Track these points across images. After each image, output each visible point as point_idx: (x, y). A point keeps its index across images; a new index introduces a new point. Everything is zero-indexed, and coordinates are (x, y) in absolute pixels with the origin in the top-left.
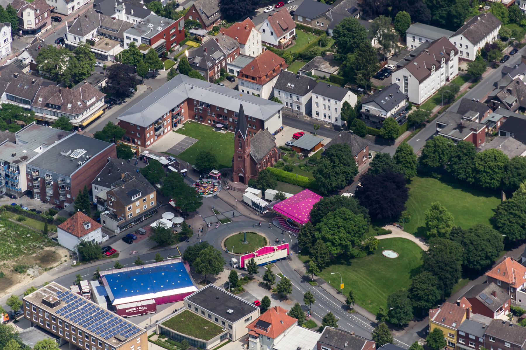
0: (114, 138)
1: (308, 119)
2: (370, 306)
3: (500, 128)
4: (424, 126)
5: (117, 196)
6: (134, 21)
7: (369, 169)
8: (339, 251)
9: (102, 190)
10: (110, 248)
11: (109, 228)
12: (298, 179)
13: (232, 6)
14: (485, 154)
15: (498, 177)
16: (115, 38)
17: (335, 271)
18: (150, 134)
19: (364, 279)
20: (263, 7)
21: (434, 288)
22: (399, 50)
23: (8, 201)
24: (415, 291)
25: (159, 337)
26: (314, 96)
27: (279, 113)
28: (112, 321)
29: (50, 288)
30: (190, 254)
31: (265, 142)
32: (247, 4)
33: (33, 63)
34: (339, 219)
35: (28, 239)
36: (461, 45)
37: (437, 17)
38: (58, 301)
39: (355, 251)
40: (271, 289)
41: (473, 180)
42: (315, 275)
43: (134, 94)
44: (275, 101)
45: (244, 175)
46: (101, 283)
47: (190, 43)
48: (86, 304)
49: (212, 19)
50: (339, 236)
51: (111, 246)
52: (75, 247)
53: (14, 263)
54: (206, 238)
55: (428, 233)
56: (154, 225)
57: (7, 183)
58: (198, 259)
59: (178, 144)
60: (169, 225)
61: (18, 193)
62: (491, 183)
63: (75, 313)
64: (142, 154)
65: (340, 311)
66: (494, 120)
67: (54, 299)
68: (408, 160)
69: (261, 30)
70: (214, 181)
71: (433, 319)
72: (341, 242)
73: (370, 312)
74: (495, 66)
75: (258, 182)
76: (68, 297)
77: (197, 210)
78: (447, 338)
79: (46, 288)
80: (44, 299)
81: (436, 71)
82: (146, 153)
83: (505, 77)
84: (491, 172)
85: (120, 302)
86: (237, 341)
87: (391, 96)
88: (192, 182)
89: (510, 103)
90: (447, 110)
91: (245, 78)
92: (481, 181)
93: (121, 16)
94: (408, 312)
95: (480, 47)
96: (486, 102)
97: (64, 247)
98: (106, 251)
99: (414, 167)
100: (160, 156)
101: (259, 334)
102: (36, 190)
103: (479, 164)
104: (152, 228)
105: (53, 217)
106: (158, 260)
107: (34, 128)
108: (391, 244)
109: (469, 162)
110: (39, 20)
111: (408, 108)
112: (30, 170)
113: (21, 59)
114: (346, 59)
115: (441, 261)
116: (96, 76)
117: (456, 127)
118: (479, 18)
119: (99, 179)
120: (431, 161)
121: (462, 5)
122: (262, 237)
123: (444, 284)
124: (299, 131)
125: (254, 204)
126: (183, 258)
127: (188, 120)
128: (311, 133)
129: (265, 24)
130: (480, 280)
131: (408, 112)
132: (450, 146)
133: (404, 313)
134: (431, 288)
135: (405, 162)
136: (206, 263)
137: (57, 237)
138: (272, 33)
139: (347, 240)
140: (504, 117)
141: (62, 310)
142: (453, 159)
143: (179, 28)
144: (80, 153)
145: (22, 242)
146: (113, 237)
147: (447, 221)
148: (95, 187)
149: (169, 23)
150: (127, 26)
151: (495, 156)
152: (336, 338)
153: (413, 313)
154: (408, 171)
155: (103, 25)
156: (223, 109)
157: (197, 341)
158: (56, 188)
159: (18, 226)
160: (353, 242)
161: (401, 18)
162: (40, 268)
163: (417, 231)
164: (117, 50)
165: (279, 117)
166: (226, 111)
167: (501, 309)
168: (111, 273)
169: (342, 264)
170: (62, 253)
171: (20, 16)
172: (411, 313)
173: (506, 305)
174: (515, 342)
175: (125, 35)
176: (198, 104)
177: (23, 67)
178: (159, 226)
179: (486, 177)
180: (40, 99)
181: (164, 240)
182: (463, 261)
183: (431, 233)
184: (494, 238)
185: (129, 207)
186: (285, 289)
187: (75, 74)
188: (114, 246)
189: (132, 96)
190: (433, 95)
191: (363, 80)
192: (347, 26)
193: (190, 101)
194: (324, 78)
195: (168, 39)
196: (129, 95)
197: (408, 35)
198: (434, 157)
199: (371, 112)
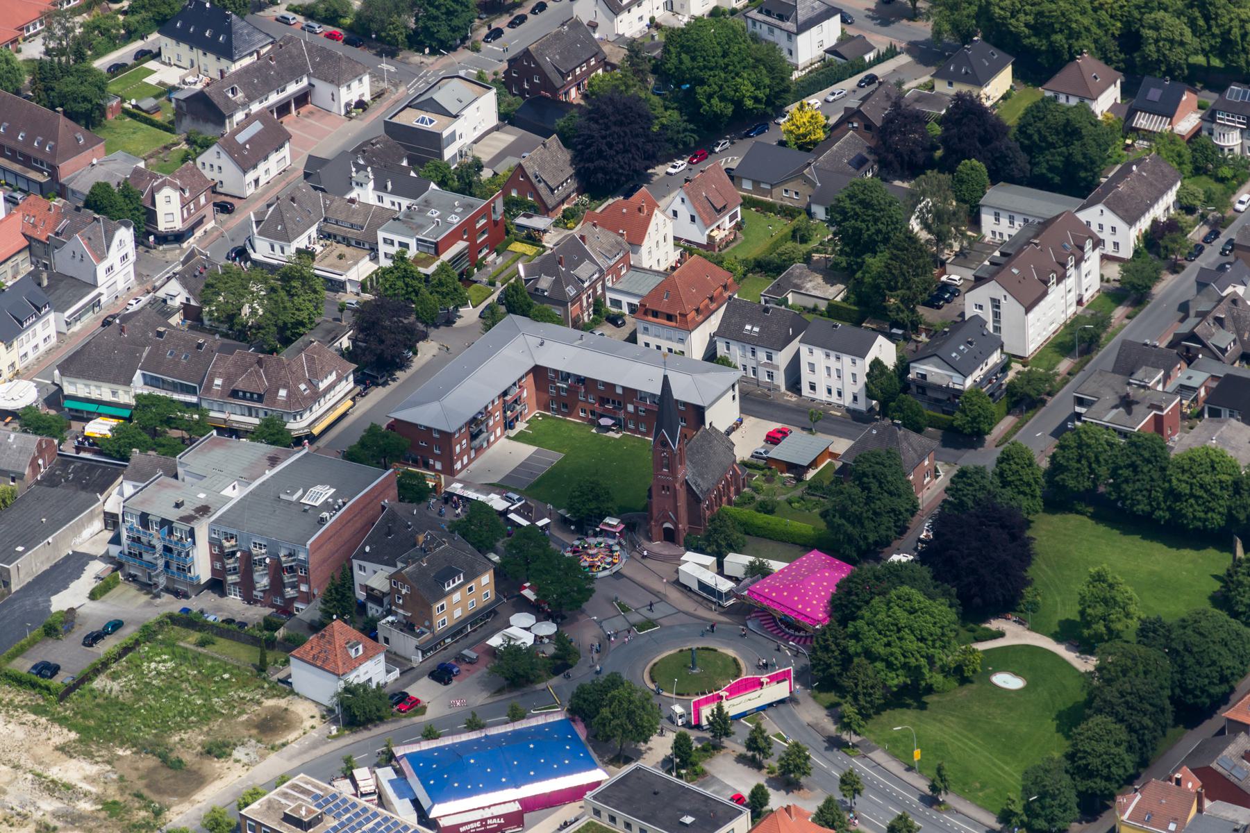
0: (385, 458)
1: (794, 398)
2: (981, 794)
3: (1206, 402)
4: (1043, 402)
5: (414, 584)
6: (393, 204)
7: (945, 501)
8: (902, 679)
9: (375, 572)
11: (398, 652)
12: (790, 529)
13: (602, 163)
14: (1190, 459)
15: (1221, 506)
17: (901, 723)
18: (461, 446)
19: (959, 736)
20: (663, 163)
21: (1121, 750)
22: (970, 244)
23: (172, 603)
24: (1081, 758)
26: (804, 350)
29: (295, 787)
30: (585, 700)
31: (715, 453)
32: (633, 158)
33: (190, 305)
35: (226, 684)
36: (1101, 226)
37: (1043, 169)
38: (317, 816)
39: (937, 679)
40: (764, 767)
41: (1167, 515)
42: (855, 733)
43: (412, 361)
44: (723, 364)
45: (676, 525)
46: (398, 771)
47: (518, 247)
48: (379, 819)
50: (901, 647)
51: (406, 690)
52: (332, 698)
53: (201, 738)
54: (607, 666)
55: (1086, 632)
56: (496, 641)
57: (167, 565)
58: (605, 712)
59: (521, 465)
60: (528, 639)
61: (192, 585)
62: (1206, 520)
64: (448, 490)
65: (917, 808)
67: (309, 811)
68: (1025, 479)
69: (671, 214)
70: (611, 542)
71: (1125, 817)
72: (907, 660)
73: (984, 807)
74: (1175, 268)
75: (707, 539)
76: (337, 806)
77: (585, 605)
79: (287, 787)
80: (287, 811)
82: (457, 488)
83: (1205, 290)
84: (1205, 495)
87: (970, 343)
88: (564, 545)
89: (1223, 347)
90: (1086, 368)
91: (650, 318)
92: (1184, 516)
93: (366, 194)
94: (1069, 804)
96: (1172, 345)
97: (307, 699)
98: (396, 704)
99: (1038, 492)
100: (489, 494)
102: (232, 578)
103: (1179, 481)
104: (493, 652)
105: (276, 634)
106: (515, 716)
107: (215, 444)
108: (1010, 659)
109: (1156, 475)
110: (189, 210)
111: (1005, 368)
112: (216, 536)
113: (164, 296)
114: (861, 267)
115: (1129, 690)
117: (1117, 402)
118: (1134, 168)
119: (367, 549)
120: (1073, 478)
121: (1095, 140)
122: (728, 656)
123: (1139, 741)
124: (778, 426)
125: (702, 585)
126: (568, 710)
127: (536, 412)
128: (803, 429)
129: (678, 200)
130: (1209, 727)
131: (1007, 375)
132: (1111, 445)
134: (1114, 750)
135: (1018, 483)
136: (624, 719)
137: (289, 676)
138: (693, 219)
139: (918, 656)
140: (1214, 377)
142: (1120, 472)
143: (494, 217)
144: (321, 494)
145: (214, 691)
147: (1127, 604)
148: (360, 566)
149: (472, 206)
150: (381, 217)
151: (1212, 461)
153: (1078, 805)
154: (1025, 502)
155: (329, 216)
158: (277, 571)
159: (200, 658)
161: (968, 175)
162: (259, 745)
163: (1058, 629)
164: (363, 269)
166: (619, 391)
168: (418, 749)
169: (908, 706)
170: (304, 711)
171: (148, 205)
172: (1074, 806)
175: (381, 235)
176: (557, 377)
177: (170, 314)
178: (508, 645)
179: (1196, 507)
180: (218, 381)
181: (521, 673)
182: (1172, 690)
183: (1092, 632)
184: (1234, 636)
185: (439, 605)
186: (797, 767)
187: (285, 324)
188: (413, 691)
189: (408, 367)
190: (1053, 336)
191: (903, 311)
192: (861, 196)
193: (539, 373)
194: (814, 310)
195: (472, 239)
196: (403, 364)
197: (983, 210)
198: (1078, 469)
199: (930, 379)
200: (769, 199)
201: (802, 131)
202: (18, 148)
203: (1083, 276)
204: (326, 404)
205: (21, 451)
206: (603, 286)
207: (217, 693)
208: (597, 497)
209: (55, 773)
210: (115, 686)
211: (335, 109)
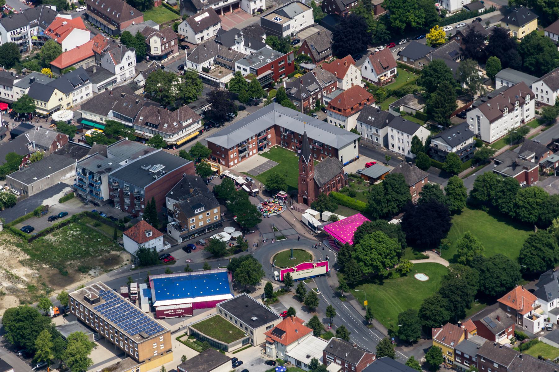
8: (370, 271)
10: (169, 256)
12: (357, 204)
13: (341, 43)
16: (230, 67)
18: (234, 155)
25: (189, 338)
27: (355, 143)
28: (142, 319)
31: (331, 168)
32: (356, 43)
34: (373, 241)
37: (527, 64)
41: (514, 214)
45: (307, 197)
46: (149, 287)
49: (323, 54)
58: (238, 270)
62: (529, 218)
63: (110, 310)
67: (93, 296)
70: (280, 201)
78: (445, 355)
80: (85, 296)
81: (509, 113)
84: (529, 207)
85: (160, 304)
86: (258, 346)
87: (459, 133)
91: (332, 110)
92: (520, 215)
101: (274, 341)
102: (116, 200)
103: (520, 200)
105: (125, 224)
110: (165, 47)
116: (202, 100)
117: (511, 164)
119: (172, 193)
123: (454, 307)
124: (373, 161)
132: (499, 181)
133: (412, 331)
135: (454, 194)
136: (245, 274)
138: (372, 71)
141: (100, 307)
143: (288, 62)
146: (175, 246)
150: (240, 57)
151: (535, 193)
152: (339, 348)
154: (457, 203)
157: (221, 344)
165: (355, 147)
167: (504, 333)
169: (375, 283)
170: (125, 257)
171: (148, 43)
173: (510, 330)
174: (502, 362)
175: (236, 64)
180: (141, 118)
182: (480, 287)
185: (191, 219)
188: (173, 254)
191: (441, 118)
192: (434, 67)
193: (276, 128)
194: (411, 114)
195: (275, 72)
196: (230, 119)
197: (497, 79)
199: (439, 147)
200: (413, 66)
201: (434, 38)
202: (107, 14)
203: (525, 111)
205: (49, 138)
206: (322, 95)
207: (92, 246)
208: (277, 182)
209: (14, 272)
210: (53, 239)
211: (249, 12)
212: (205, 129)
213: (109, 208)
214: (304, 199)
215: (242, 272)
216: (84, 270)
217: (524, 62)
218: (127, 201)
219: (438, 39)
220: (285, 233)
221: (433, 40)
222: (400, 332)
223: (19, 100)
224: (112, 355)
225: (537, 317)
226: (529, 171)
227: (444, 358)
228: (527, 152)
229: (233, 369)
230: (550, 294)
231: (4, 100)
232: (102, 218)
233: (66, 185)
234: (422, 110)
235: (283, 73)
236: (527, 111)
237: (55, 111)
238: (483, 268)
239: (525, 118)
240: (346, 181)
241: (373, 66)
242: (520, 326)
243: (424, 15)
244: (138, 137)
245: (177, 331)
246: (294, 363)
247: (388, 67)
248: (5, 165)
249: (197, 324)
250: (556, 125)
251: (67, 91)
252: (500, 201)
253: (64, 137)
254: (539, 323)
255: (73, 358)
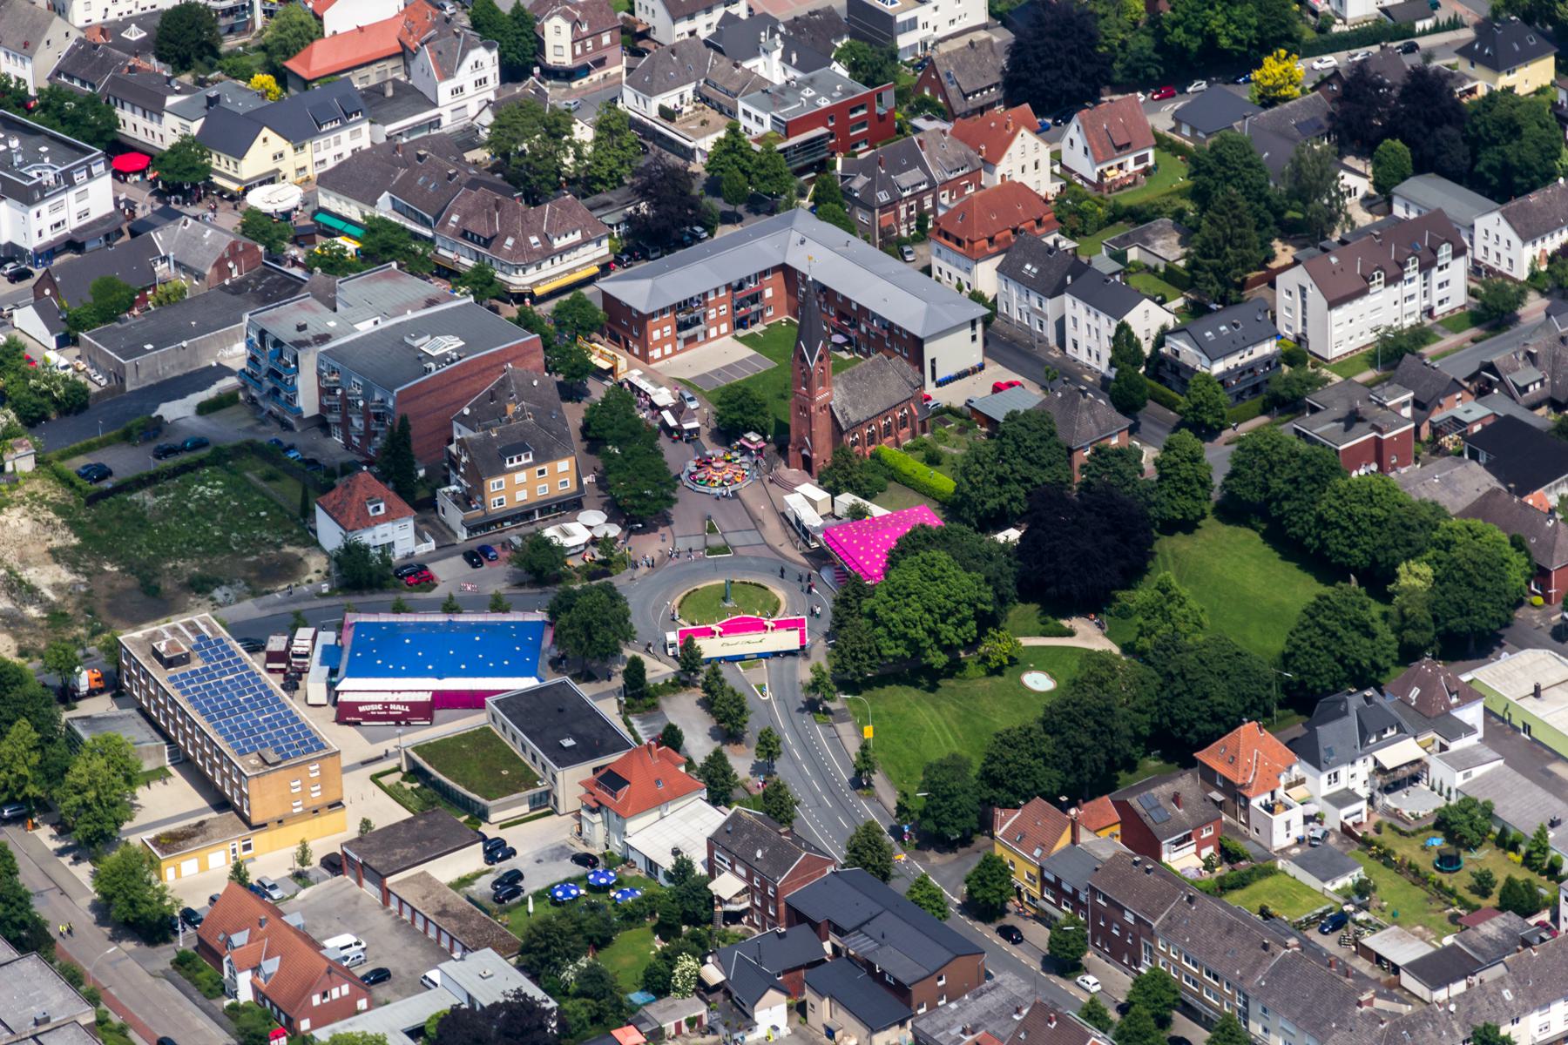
8: (901, 651)
10: (422, 568)
12: (933, 482)
25: (404, 779)
66: (1467, 418)
81: (1386, 285)
87: (1236, 326)
91: (942, 239)
95: (1543, 251)
101: (601, 805)
110: (584, 47)
133: (954, 811)
141: (184, 676)
152: (746, 836)
156: (848, 301)
160: (931, 632)
165: (974, 338)
167: (1188, 838)
169: (917, 685)
174: (1143, 911)
180: (455, 218)
182: (1160, 717)
185: (495, 481)
188: (433, 568)
194: (1153, 271)
197: (1396, 199)
199: (1183, 358)
201: (1269, 82)
204: (560, 265)
205: (211, 248)
206: (935, 202)
207: (240, 530)
208: (741, 408)
209: (30, 575)
212: (619, 261)
213: (316, 436)
214: (805, 457)
215: (571, 625)
216: (201, 586)
217: (1475, 161)
218: (357, 422)
219: (1281, 87)
220: (733, 539)
221: (1267, 89)
222: (924, 814)
223: (174, 149)
224: (202, 803)
225: (1288, 807)
226: (1385, 437)
227: (1018, 889)
228: (1389, 390)
229: (487, 867)
230: (1330, 752)
231: (142, 147)
232: (287, 461)
233: (229, 372)
234: (1182, 263)
235: (862, 138)
236: (1441, 286)
237: (261, 184)
238: (1170, 667)
239: (1435, 303)
240: (923, 423)
241: (1088, 139)
242: (1242, 828)
243: (1253, 21)
244: (438, 267)
245: (379, 759)
246: (641, 865)
247: (1128, 145)
248: (85, 306)
249: (429, 745)
250: (1513, 330)
251: (298, 136)
252: (1286, 506)
253: (250, 250)
254: (1288, 824)
255: (78, 798)
